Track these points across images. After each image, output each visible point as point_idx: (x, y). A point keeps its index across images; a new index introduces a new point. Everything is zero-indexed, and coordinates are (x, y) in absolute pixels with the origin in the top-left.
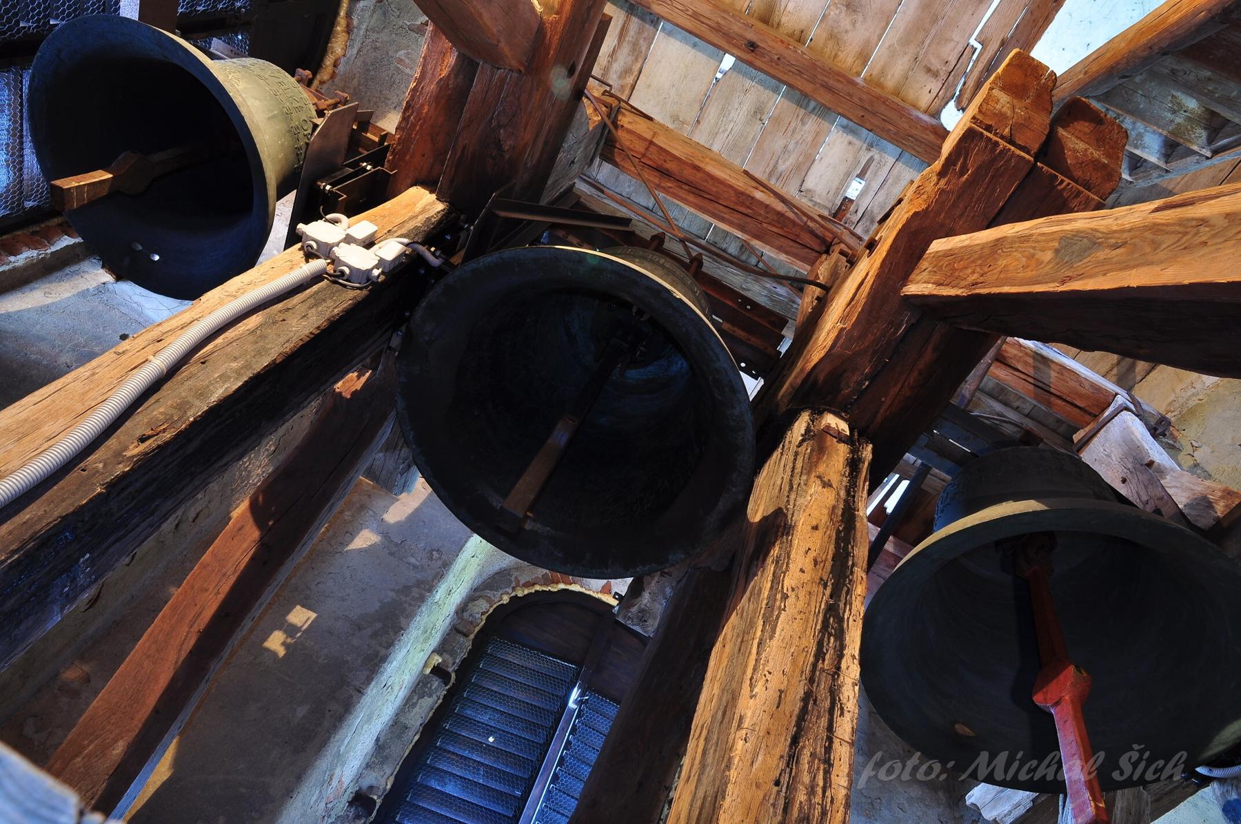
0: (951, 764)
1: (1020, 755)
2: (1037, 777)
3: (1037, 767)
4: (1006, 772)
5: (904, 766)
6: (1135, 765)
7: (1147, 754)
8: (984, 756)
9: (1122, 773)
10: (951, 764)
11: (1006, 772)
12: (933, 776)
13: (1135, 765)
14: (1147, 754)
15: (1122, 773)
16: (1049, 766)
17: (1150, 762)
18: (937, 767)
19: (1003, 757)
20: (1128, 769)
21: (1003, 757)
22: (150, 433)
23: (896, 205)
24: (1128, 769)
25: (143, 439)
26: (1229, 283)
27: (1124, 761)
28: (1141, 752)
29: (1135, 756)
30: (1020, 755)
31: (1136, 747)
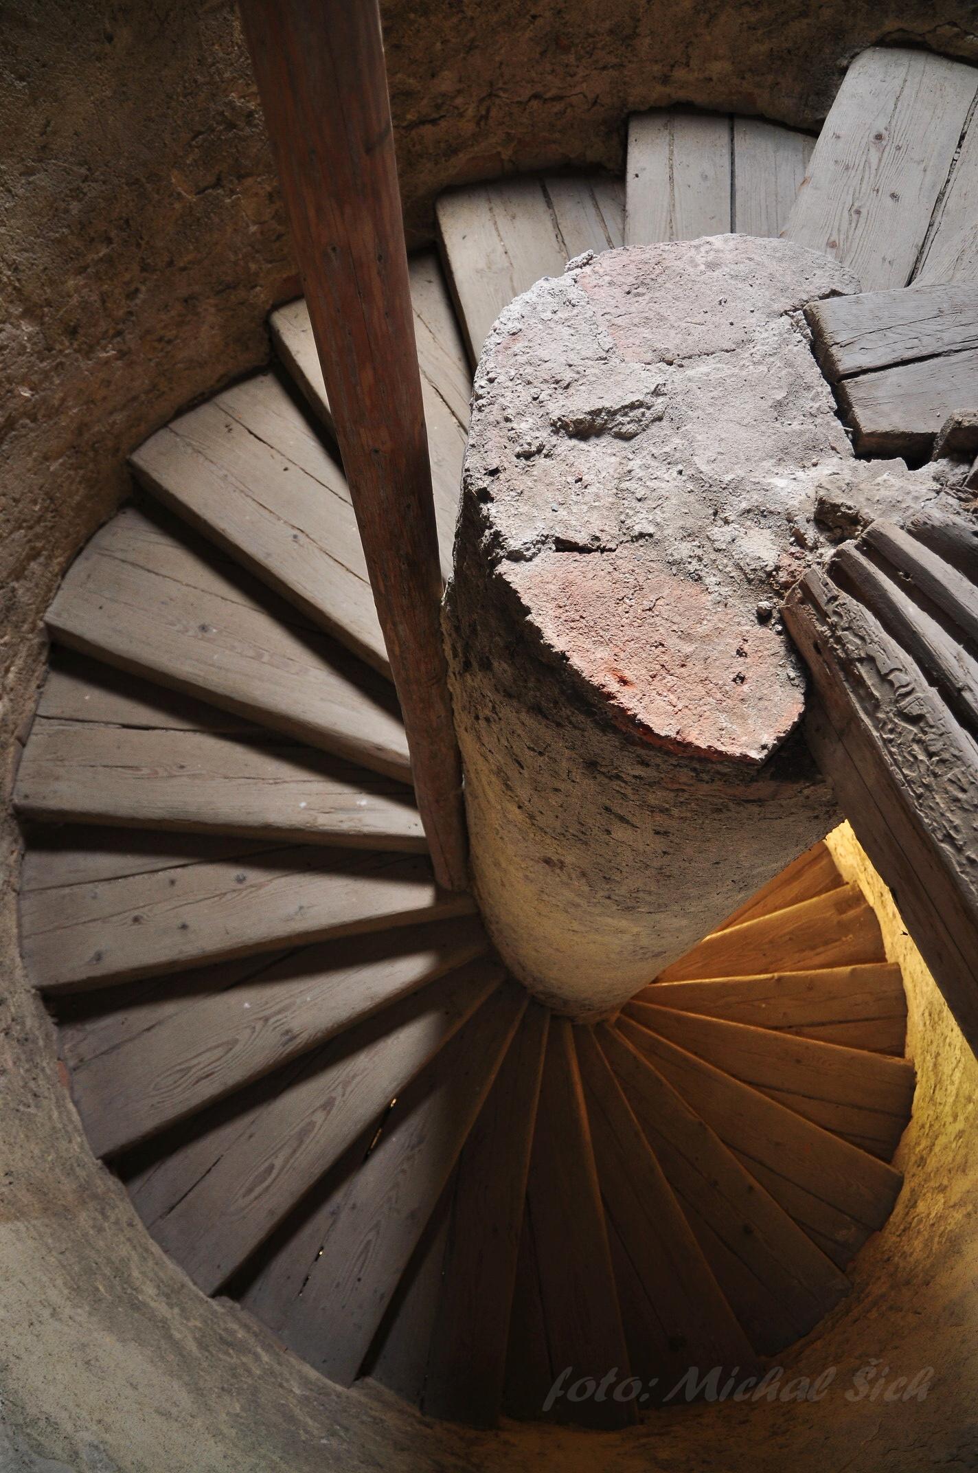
0: (653, 1382)
1: (736, 1371)
2: (906, 1397)
4: (719, 1393)
5: (598, 1385)
8: (693, 1372)
9: (856, 1394)
10: (653, 1382)
11: (719, 1393)
12: (633, 1395)
13: (872, 1383)
15: (856, 1394)
18: (637, 1386)
19: (716, 1372)
21: (716, 1372)
22: (935, 47)
23: (942, 194)
25: (474, 500)
26: (923, 610)
29: (872, 1373)
30: (736, 1371)
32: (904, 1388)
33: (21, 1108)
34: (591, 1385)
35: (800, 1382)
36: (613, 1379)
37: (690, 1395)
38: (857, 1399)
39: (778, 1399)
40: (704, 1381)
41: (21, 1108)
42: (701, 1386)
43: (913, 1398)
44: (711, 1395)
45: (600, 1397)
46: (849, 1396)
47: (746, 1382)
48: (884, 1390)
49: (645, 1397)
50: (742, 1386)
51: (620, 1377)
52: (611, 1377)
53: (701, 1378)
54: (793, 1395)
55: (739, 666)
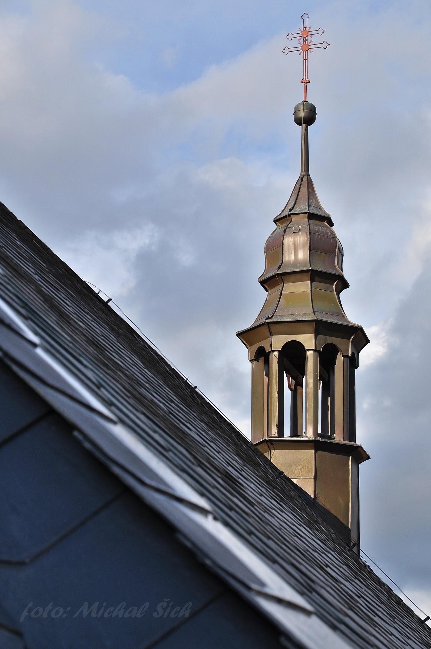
0: (68, 609)
6: (165, 609)
7: (171, 604)
8: (86, 604)
9: (158, 614)
13: (165, 609)
14: (171, 604)
15: (158, 614)
19: (95, 606)
20: (161, 612)
21: (97, 604)
27: (159, 608)
28: (168, 603)
29: (165, 604)
31: (165, 600)
35: (133, 609)
38: (159, 616)
42: (90, 610)
44: (94, 615)
46: (155, 615)
50: (108, 611)
53: (89, 607)
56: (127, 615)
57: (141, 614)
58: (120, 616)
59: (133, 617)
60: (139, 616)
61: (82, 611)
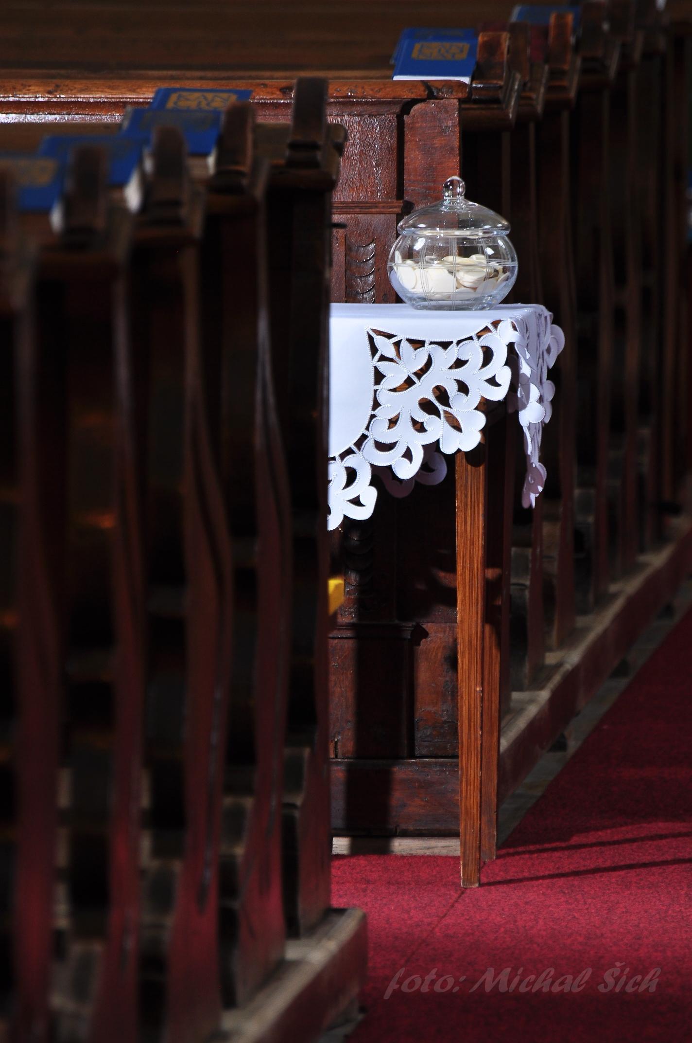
0: (462, 979)
2: (642, 988)
3: (535, 981)
6: (617, 980)
9: (606, 987)
13: (617, 980)
15: (606, 987)
16: (545, 980)
17: (629, 978)
20: (610, 981)
24: (610, 981)
28: (622, 969)
29: (617, 971)
31: (618, 964)
32: (639, 984)
33: (431, 184)
34: (418, 981)
36: (434, 977)
37: (488, 988)
39: (496, 987)
40: (497, 979)
41: (431, 184)
42: (496, 982)
43: (540, 991)
45: (425, 989)
46: (601, 988)
47: (634, 979)
48: (521, 982)
49: (456, 989)
50: (632, 982)
51: (439, 975)
52: (432, 975)
53: (496, 976)
54: (561, 988)
55: (460, 374)
56: (556, 989)
57: (579, 986)
58: (545, 990)
59: (565, 991)
60: (576, 990)
61: (483, 983)
